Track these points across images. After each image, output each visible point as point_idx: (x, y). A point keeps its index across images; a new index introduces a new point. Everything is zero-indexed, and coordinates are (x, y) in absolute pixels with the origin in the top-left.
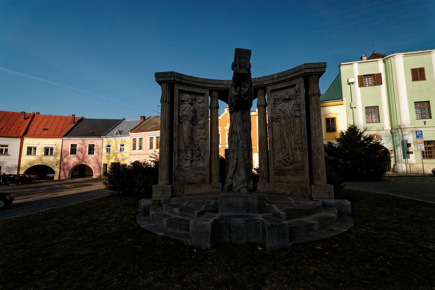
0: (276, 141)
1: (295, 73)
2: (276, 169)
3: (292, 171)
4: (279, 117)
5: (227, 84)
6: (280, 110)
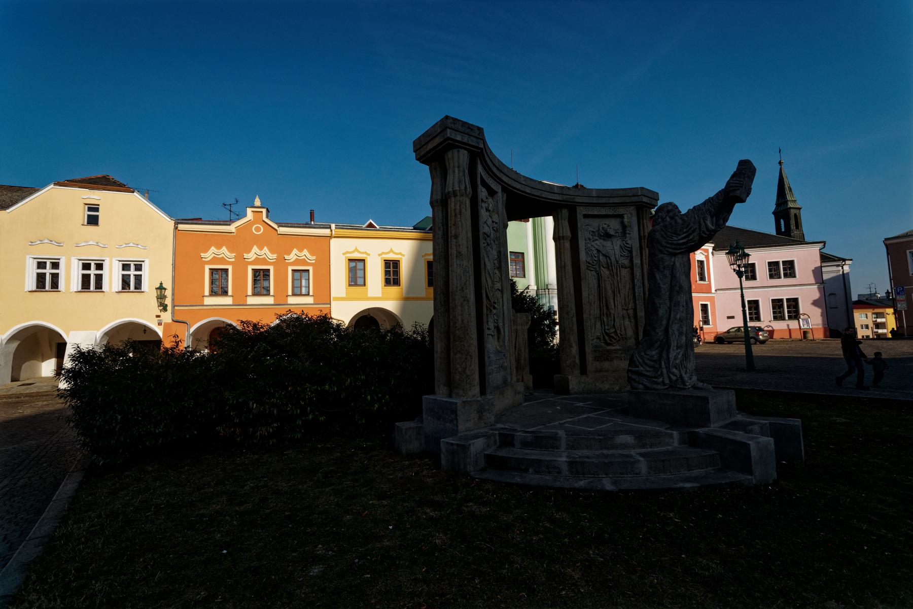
0: (593, 302)
1: (625, 198)
2: (596, 351)
3: (620, 352)
4: (595, 262)
5: (524, 183)
6: (599, 251)
